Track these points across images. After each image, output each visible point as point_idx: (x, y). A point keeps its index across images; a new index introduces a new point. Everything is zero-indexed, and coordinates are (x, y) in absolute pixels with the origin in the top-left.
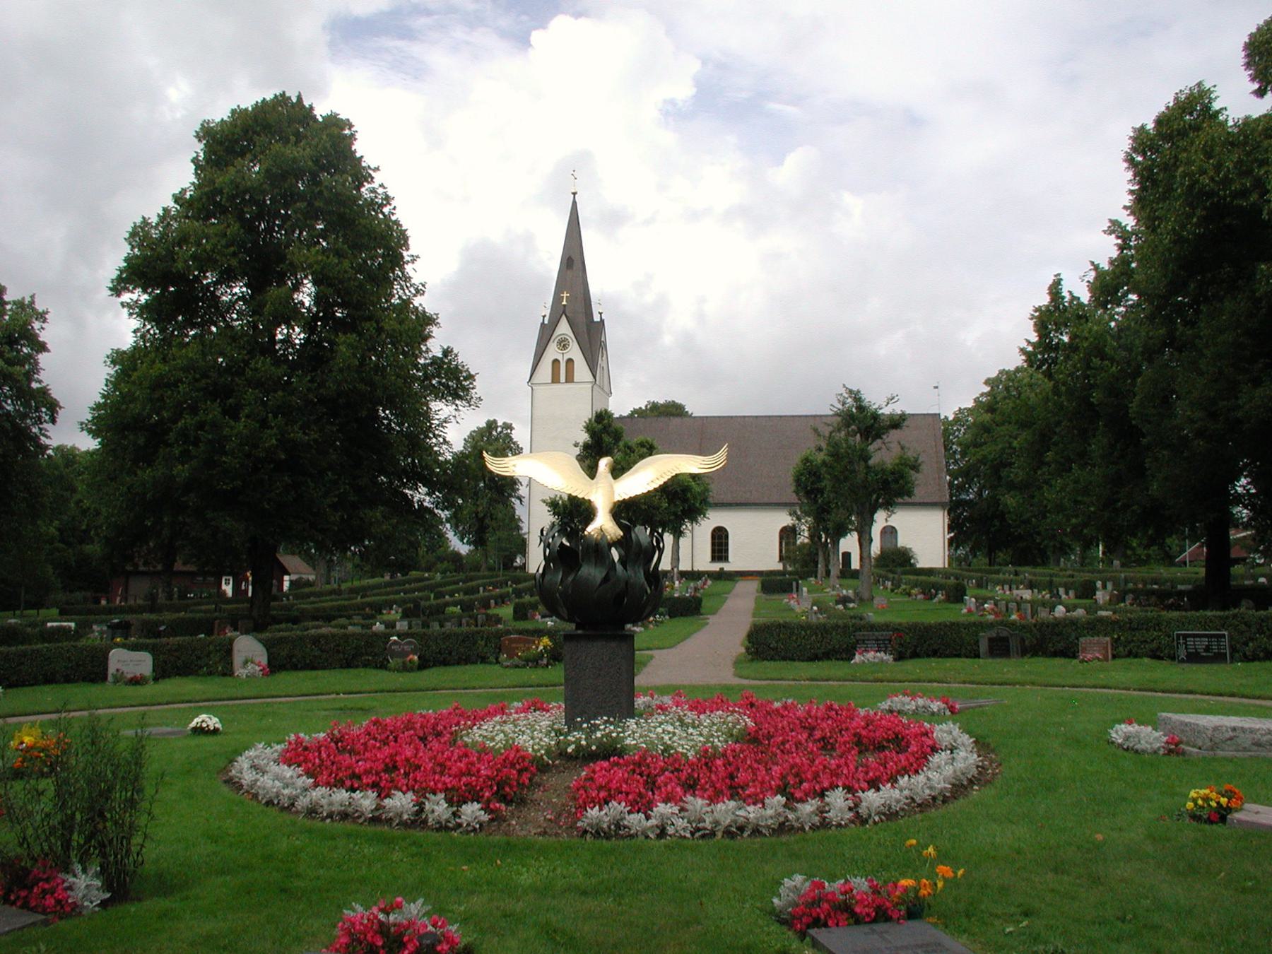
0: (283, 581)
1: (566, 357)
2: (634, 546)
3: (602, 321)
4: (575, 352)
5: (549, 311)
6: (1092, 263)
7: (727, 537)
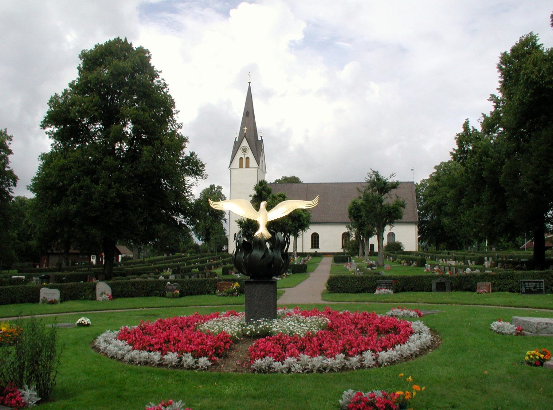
1: (246, 156)
3: (262, 140)
4: (250, 154)
6: (483, 114)
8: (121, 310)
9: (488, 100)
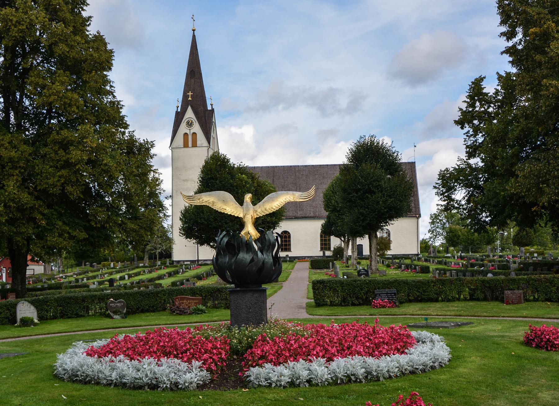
1: (192, 131)
3: (213, 110)
4: (197, 128)
5: (181, 104)
6: (485, 78)
7: (290, 237)
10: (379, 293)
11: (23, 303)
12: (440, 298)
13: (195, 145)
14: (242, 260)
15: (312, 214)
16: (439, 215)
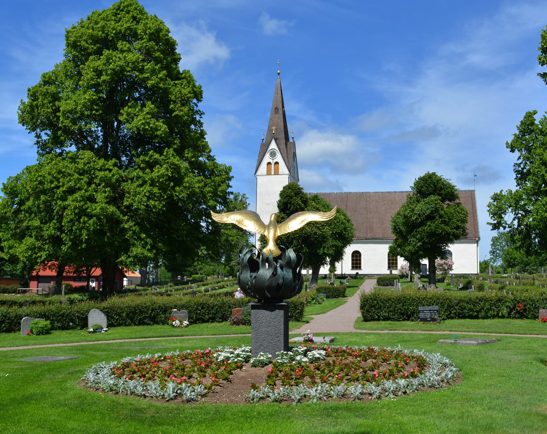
0: (123, 281)
1: (275, 161)
2: (286, 258)
4: (279, 158)
8: (105, 342)
9: (492, 230)
10: (423, 309)
11: (95, 311)
12: (480, 316)
13: (277, 173)
14: (262, 276)
15: (381, 236)
16: (499, 238)
